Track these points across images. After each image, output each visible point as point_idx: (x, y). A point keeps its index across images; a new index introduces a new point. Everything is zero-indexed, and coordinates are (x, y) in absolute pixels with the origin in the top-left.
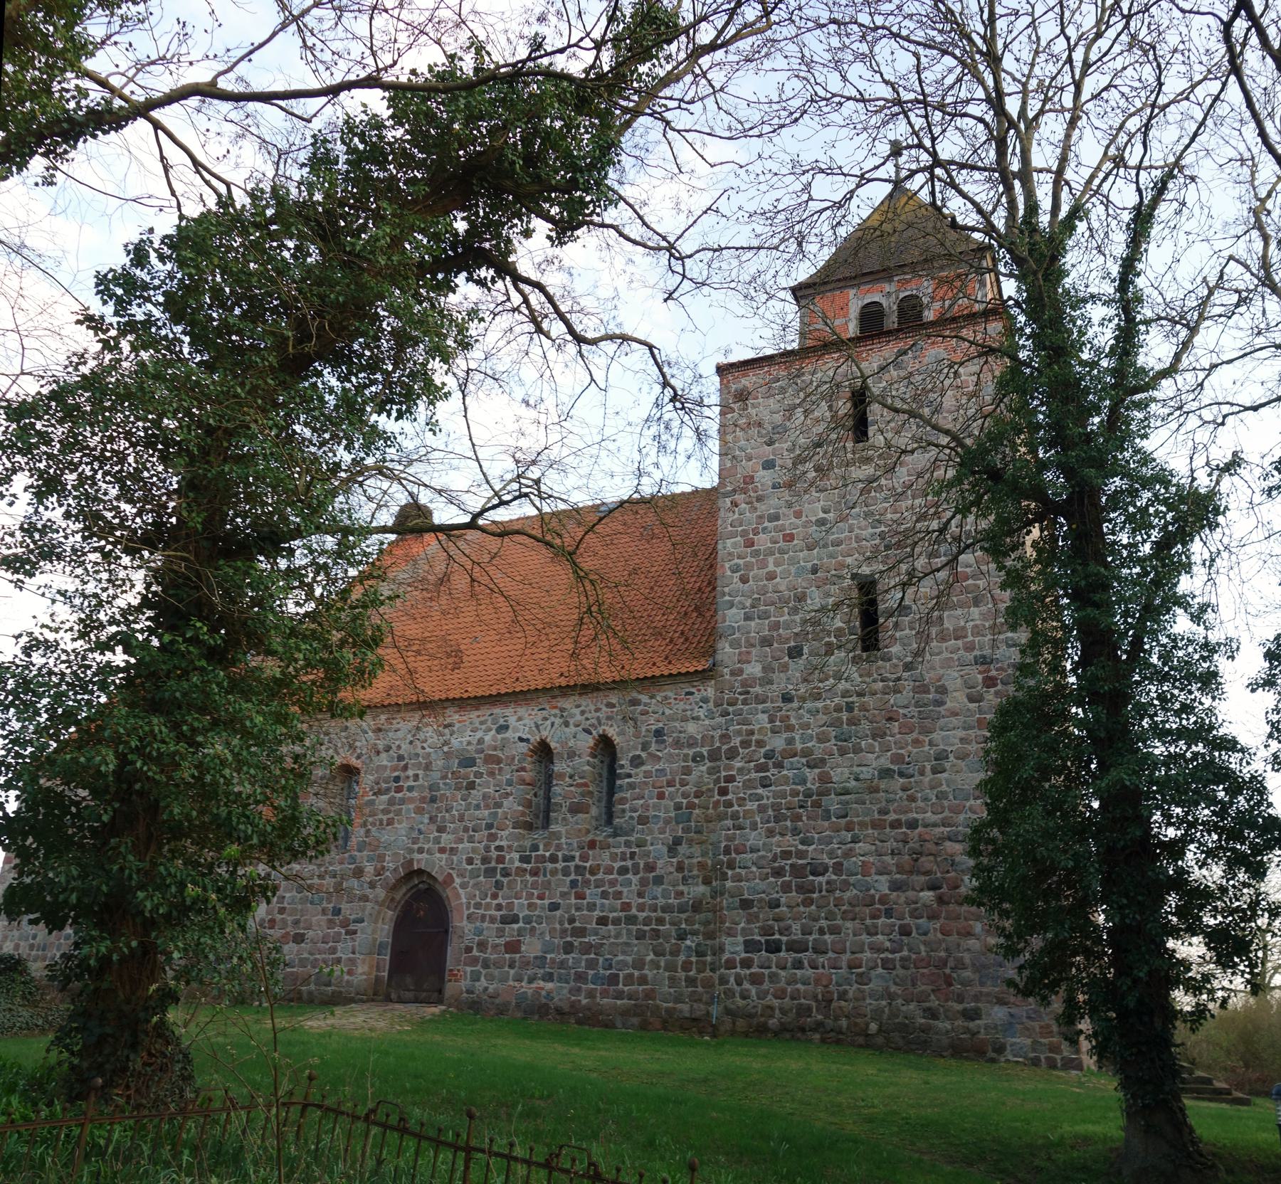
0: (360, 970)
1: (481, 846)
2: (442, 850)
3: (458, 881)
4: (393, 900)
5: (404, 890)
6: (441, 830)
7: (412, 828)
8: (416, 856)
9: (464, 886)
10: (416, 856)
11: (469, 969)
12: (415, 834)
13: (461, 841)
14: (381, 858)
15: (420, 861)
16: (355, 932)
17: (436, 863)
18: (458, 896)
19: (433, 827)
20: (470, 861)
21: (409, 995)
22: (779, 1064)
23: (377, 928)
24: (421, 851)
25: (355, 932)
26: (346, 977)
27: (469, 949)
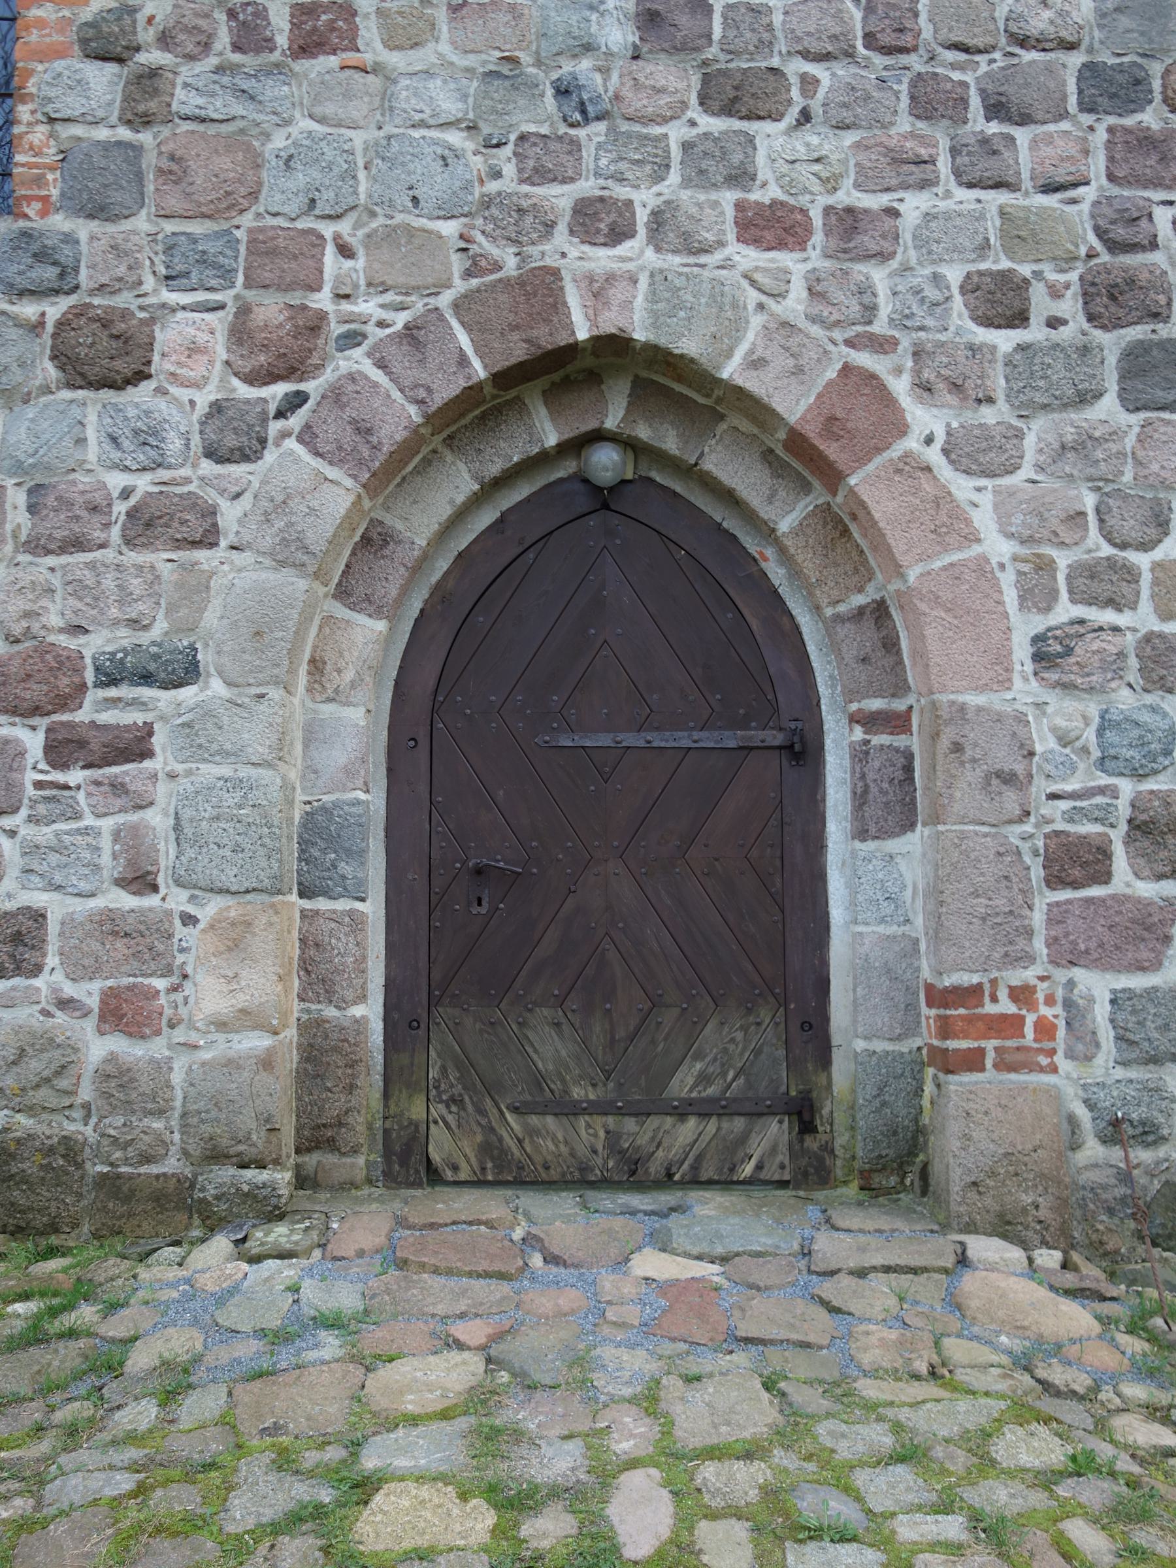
0: (210, 996)
1: (1078, 215)
2: (771, 226)
3: (927, 420)
4: (373, 541)
5: (458, 481)
6: (739, 95)
7: (506, 73)
8: (568, 254)
9: (978, 455)
10: (568, 254)
11: (1097, 986)
12: (540, 115)
13: (914, 170)
14: (283, 259)
15: (612, 291)
16: (135, 746)
17: (755, 320)
18: (951, 524)
19: (676, 78)
20: (1002, 302)
21: (553, 1137)
22: (681, 1139)
23: (285, 727)
24: (601, 222)
25: (135, 746)
26: (99, 1048)
27: (1075, 862)
